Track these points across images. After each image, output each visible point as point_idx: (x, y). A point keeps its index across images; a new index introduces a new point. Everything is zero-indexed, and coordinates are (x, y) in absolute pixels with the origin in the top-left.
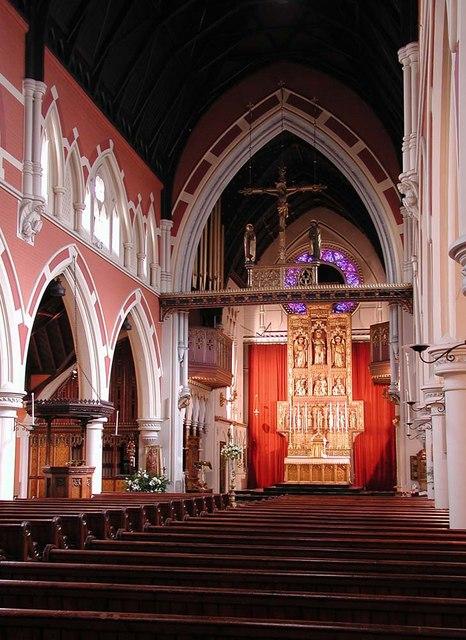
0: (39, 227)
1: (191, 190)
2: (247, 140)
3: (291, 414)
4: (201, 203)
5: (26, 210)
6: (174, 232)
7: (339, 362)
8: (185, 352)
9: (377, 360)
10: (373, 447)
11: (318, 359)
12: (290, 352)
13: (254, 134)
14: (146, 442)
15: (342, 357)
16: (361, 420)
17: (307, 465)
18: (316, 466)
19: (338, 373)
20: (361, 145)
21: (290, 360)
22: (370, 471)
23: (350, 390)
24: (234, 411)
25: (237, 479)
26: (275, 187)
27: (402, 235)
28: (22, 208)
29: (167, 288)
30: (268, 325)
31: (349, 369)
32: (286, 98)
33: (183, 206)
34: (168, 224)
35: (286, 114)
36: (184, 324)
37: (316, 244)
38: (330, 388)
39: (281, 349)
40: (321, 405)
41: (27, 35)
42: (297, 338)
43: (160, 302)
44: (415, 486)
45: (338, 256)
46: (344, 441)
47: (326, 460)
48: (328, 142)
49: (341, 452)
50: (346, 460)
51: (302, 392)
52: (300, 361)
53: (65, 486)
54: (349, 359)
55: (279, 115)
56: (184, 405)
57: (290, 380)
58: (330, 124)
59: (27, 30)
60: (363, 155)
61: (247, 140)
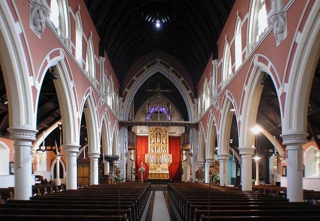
1: (129, 88)
2: (147, 73)
3: (150, 158)
4: (131, 93)
5: (100, 98)
6: (123, 101)
7: (165, 142)
9: (184, 143)
10: (175, 168)
11: (158, 141)
12: (149, 139)
13: (149, 72)
14: (115, 167)
15: (165, 141)
16: (171, 160)
17: (156, 174)
18: (158, 174)
19: (164, 146)
20: (182, 79)
21: (149, 141)
22: (173, 176)
23: (168, 151)
25: (124, 181)
28: (99, 97)
29: (121, 119)
30: (141, 131)
31: (168, 145)
33: (126, 93)
37: (169, 108)
39: (146, 138)
40: (158, 155)
44: (197, 180)
45: (164, 109)
46: (166, 166)
47: (161, 172)
48: (91, 44)
49: (166, 169)
50: (168, 172)
51: (153, 151)
52: (152, 142)
53: (107, 180)
54: (168, 141)
55: (157, 66)
56: (127, 156)
57: (149, 148)
58: (173, 71)
60: (183, 82)
61: (147, 73)
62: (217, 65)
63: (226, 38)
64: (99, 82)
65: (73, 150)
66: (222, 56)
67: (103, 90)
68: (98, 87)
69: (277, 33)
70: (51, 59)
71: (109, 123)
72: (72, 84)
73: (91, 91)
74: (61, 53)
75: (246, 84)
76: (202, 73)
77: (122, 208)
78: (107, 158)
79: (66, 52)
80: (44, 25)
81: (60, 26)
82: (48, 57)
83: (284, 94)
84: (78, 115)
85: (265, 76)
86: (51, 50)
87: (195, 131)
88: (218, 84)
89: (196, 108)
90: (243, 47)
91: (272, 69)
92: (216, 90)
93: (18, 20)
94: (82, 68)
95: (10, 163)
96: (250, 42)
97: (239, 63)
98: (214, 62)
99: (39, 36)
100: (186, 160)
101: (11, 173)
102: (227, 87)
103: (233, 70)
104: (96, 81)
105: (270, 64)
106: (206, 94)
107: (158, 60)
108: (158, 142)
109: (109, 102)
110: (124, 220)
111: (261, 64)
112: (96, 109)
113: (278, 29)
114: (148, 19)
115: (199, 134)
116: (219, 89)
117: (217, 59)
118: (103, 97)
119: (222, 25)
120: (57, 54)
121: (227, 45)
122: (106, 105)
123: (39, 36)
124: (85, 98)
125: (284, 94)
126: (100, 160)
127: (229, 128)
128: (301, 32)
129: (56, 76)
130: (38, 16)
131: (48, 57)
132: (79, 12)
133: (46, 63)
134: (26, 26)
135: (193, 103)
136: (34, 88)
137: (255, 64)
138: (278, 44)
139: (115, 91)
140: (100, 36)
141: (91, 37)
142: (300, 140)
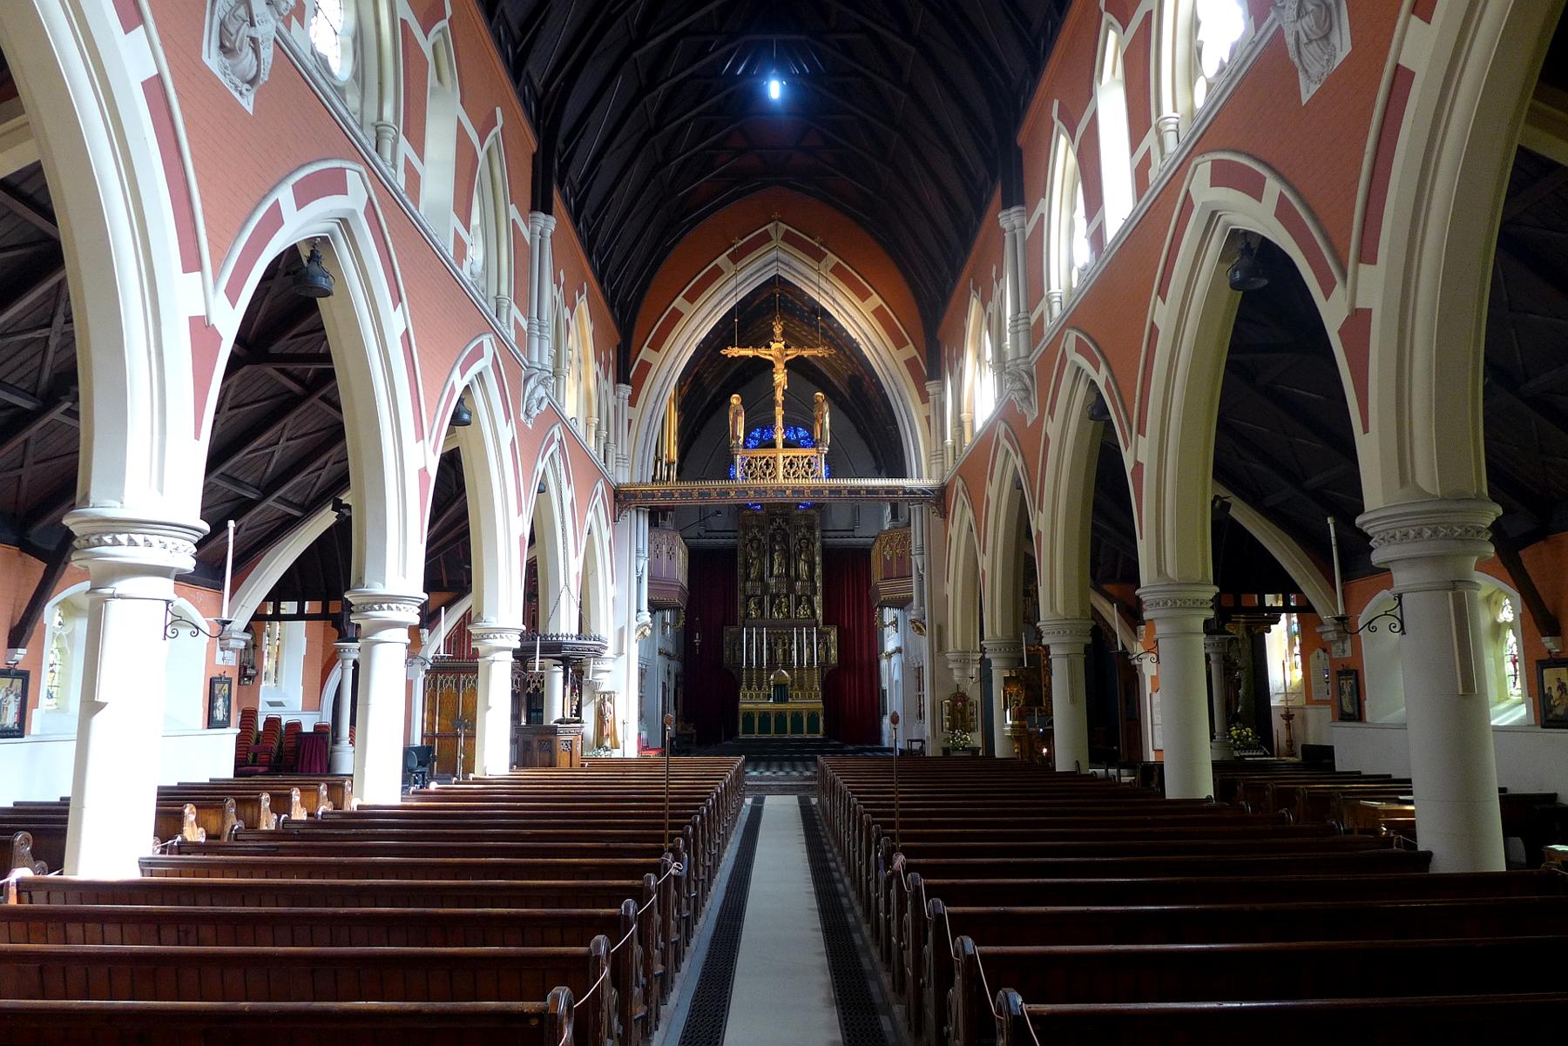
0: (544, 406)
2: (733, 283)
6: (633, 401)
8: (644, 564)
13: (740, 277)
14: (594, 687)
21: (740, 571)
24: (1242, 620)
26: (768, 347)
27: (928, 418)
28: (526, 380)
29: (623, 477)
32: (780, 235)
33: (645, 367)
34: (626, 390)
35: (781, 255)
36: (644, 523)
38: (792, 608)
41: (534, 156)
42: (751, 541)
43: (616, 496)
59: (535, 150)
62: (1023, 227)
63: (1055, 114)
64: (528, 317)
65: (386, 614)
66: (1042, 190)
67: (542, 354)
68: (524, 338)
69: (1304, 39)
70: (300, 206)
71: (568, 495)
72: (396, 321)
73: (488, 351)
74: (353, 179)
75: (1162, 292)
76: (956, 273)
77: (672, 826)
78: (554, 649)
79: (377, 179)
80: (267, 53)
81: (359, 75)
82: (285, 195)
83: (1358, 321)
84: (424, 458)
85: (1247, 250)
86: (302, 166)
87: (936, 519)
88: (1030, 308)
89: (935, 421)
90: (1136, 137)
91: (1284, 212)
92: (1021, 336)
93: (141, 20)
94: (450, 253)
95: (212, 682)
96: (1167, 109)
97: (1120, 205)
98: (1008, 220)
99: (248, 103)
100: (899, 650)
101: (211, 723)
102: (1073, 319)
103: (1097, 237)
104: (515, 311)
105: (1273, 187)
106: (979, 357)
107: (778, 229)
108: (775, 572)
109: (571, 406)
110: (550, 1023)
111: (1227, 196)
112: (507, 432)
113: (1308, 21)
114: (735, 66)
115: (953, 531)
116: (1035, 332)
117: (1021, 202)
118: (543, 382)
119: (1036, 60)
120: (334, 184)
121: (1063, 140)
122: (554, 414)
123: (248, 103)
124: (459, 382)
125: (1358, 321)
126: (522, 657)
127: (1493, 217)
128: (1427, 19)
129: (323, 282)
130: (242, 11)
131: (285, 195)
132: (444, 23)
133: (274, 220)
134: (178, 46)
135: (924, 397)
136: (202, 329)
137: (1197, 202)
138: (1307, 91)
139: (597, 358)
140: (537, 128)
141: (497, 129)
142: (1164, 611)
